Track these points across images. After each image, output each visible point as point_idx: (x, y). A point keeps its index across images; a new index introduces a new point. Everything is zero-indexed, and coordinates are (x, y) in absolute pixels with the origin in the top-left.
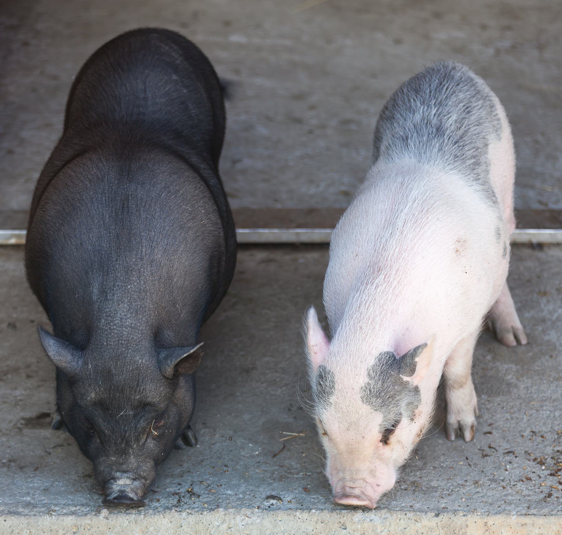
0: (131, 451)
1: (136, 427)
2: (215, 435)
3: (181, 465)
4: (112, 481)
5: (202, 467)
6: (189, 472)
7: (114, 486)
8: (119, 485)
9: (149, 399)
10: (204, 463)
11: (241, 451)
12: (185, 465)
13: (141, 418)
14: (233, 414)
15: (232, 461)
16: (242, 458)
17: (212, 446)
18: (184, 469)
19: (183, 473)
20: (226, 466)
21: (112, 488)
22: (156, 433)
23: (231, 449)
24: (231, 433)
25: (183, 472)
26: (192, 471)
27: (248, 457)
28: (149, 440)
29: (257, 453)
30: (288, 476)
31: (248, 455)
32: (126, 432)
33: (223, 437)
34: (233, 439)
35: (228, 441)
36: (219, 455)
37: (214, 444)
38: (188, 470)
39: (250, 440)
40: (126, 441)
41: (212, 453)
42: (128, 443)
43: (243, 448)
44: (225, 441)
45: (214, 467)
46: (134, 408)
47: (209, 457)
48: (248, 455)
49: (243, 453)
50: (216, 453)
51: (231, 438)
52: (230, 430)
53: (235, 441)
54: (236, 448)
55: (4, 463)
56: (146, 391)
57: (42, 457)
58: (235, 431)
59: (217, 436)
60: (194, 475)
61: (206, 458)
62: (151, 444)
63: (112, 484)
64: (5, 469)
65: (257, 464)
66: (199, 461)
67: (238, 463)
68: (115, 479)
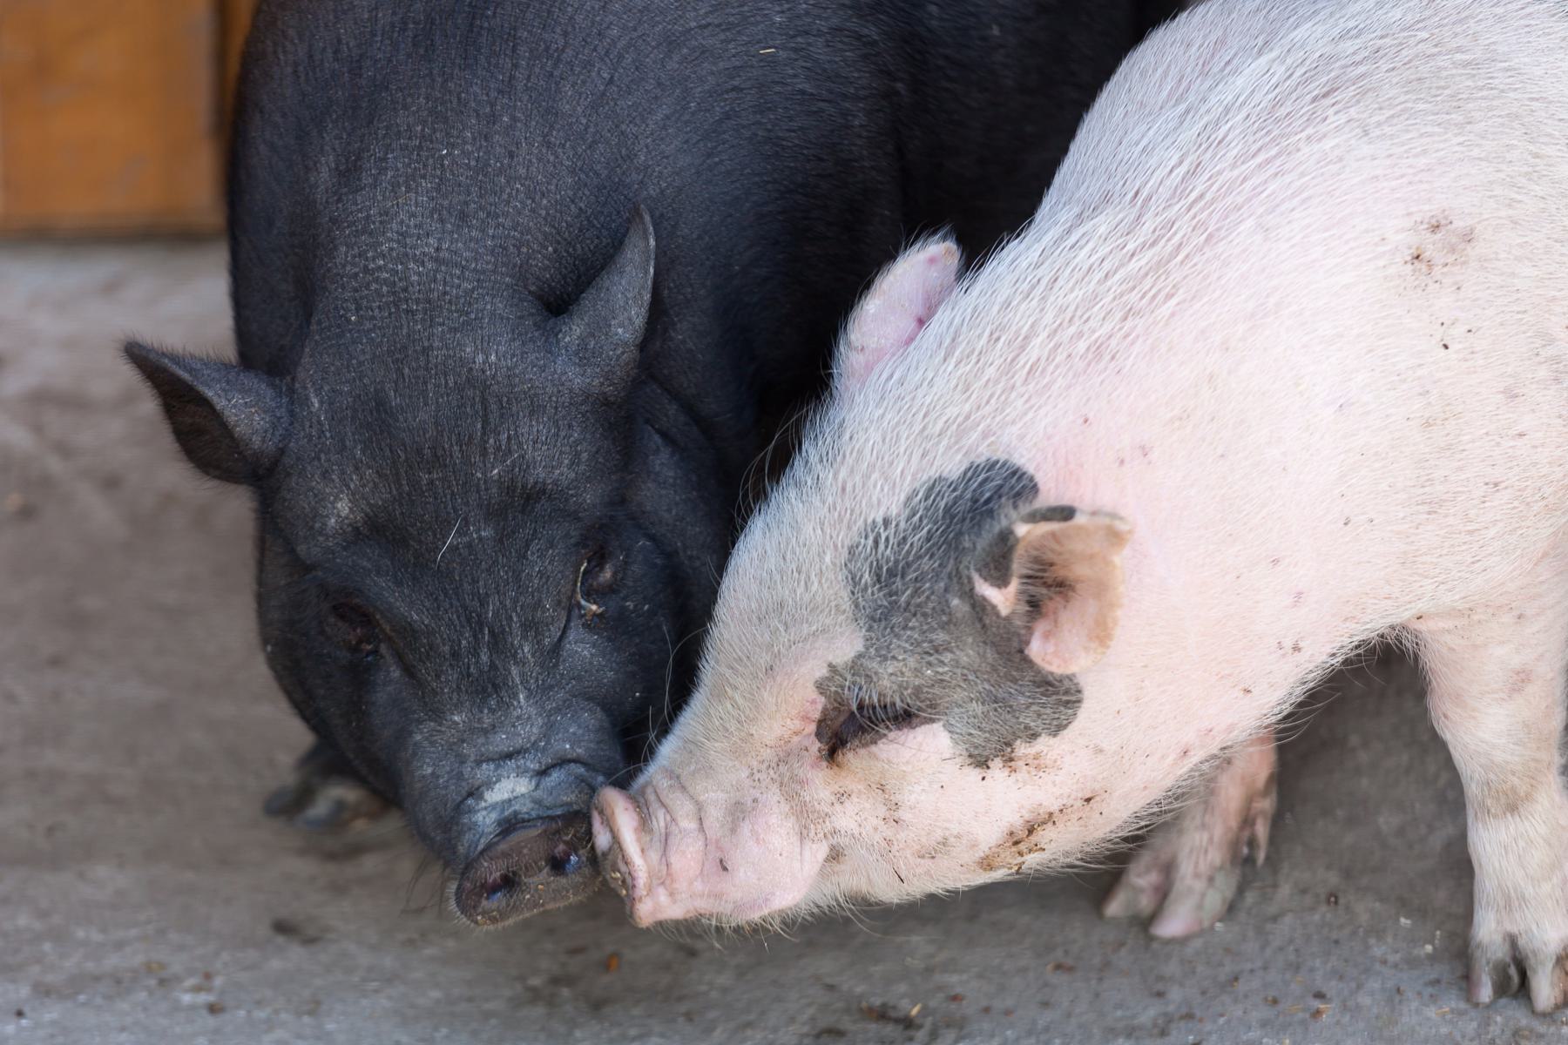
0: (514, 671)
1: (517, 578)
2: (1275, 886)
3: (1160, 994)
4: (470, 801)
5: (1236, 1001)
6: (1189, 1016)
7: (479, 817)
8: (494, 807)
9: (539, 473)
10: (1241, 987)
11: (1372, 941)
12: (1175, 994)
13: (527, 546)
14: (1340, 813)
15: (1341, 978)
16: (1378, 966)
17: (1269, 926)
18: (1171, 1008)
19: (1170, 1021)
20: (1320, 996)
21: (475, 824)
22: (594, 607)
23: (1334, 936)
24: (1333, 879)
25: (1169, 1019)
26: (1198, 1014)
27: (1396, 966)
28: (571, 636)
29: (1429, 948)
30: (1542, 1029)
31: (1397, 957)
32: (483, 603)
33: (1304, 891)
34: (1342, 901)
35: (1324, 908)
36: (1292, 957)
37: (1274, 919)
38: (1184, 1010)
39: (1403, 905)
40: (492, 632)
41: (1268, 952)
42: (498, 642)
43: (1380, 934)
44: (1313, 909)
45: (1275, 1002)
46: (495, 514)
47: (1259, 964)
48: (1397, 957)
49: (1378, 951)
50: (1281, 949)
51: (1333, 898)
52: (1329, 867)
53: (1347, 908)
54: (1354, 933)
55: (534, 990)
56: (520, 445)
57: (667, 967)
58: (1347, 874)
59: (1285, 890)
60: (1208, 1027)
61: (1249, 966)
62: (582, 649)
63: (471, 811)
64: (539, 1011)
65: (1430, 990)
66: (1222, 978)
67: (1359, 987)
68: (475, 793)
